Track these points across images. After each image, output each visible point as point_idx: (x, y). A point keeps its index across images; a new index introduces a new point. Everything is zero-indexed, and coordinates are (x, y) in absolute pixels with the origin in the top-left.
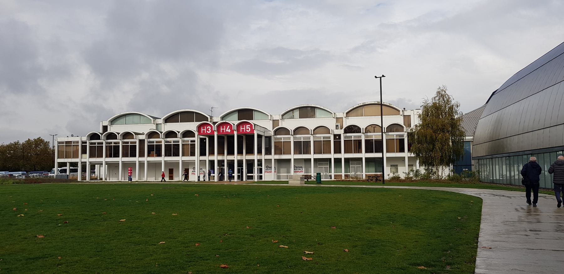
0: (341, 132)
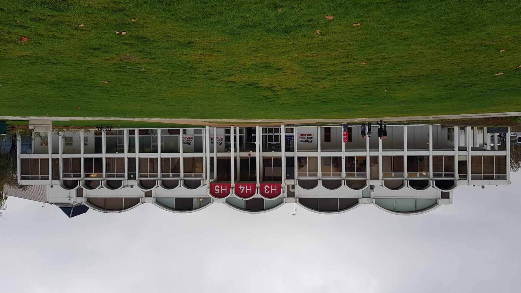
0: (370, 182)
